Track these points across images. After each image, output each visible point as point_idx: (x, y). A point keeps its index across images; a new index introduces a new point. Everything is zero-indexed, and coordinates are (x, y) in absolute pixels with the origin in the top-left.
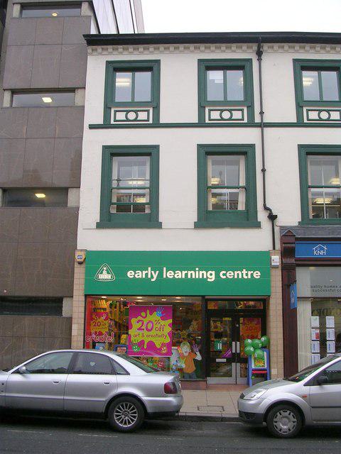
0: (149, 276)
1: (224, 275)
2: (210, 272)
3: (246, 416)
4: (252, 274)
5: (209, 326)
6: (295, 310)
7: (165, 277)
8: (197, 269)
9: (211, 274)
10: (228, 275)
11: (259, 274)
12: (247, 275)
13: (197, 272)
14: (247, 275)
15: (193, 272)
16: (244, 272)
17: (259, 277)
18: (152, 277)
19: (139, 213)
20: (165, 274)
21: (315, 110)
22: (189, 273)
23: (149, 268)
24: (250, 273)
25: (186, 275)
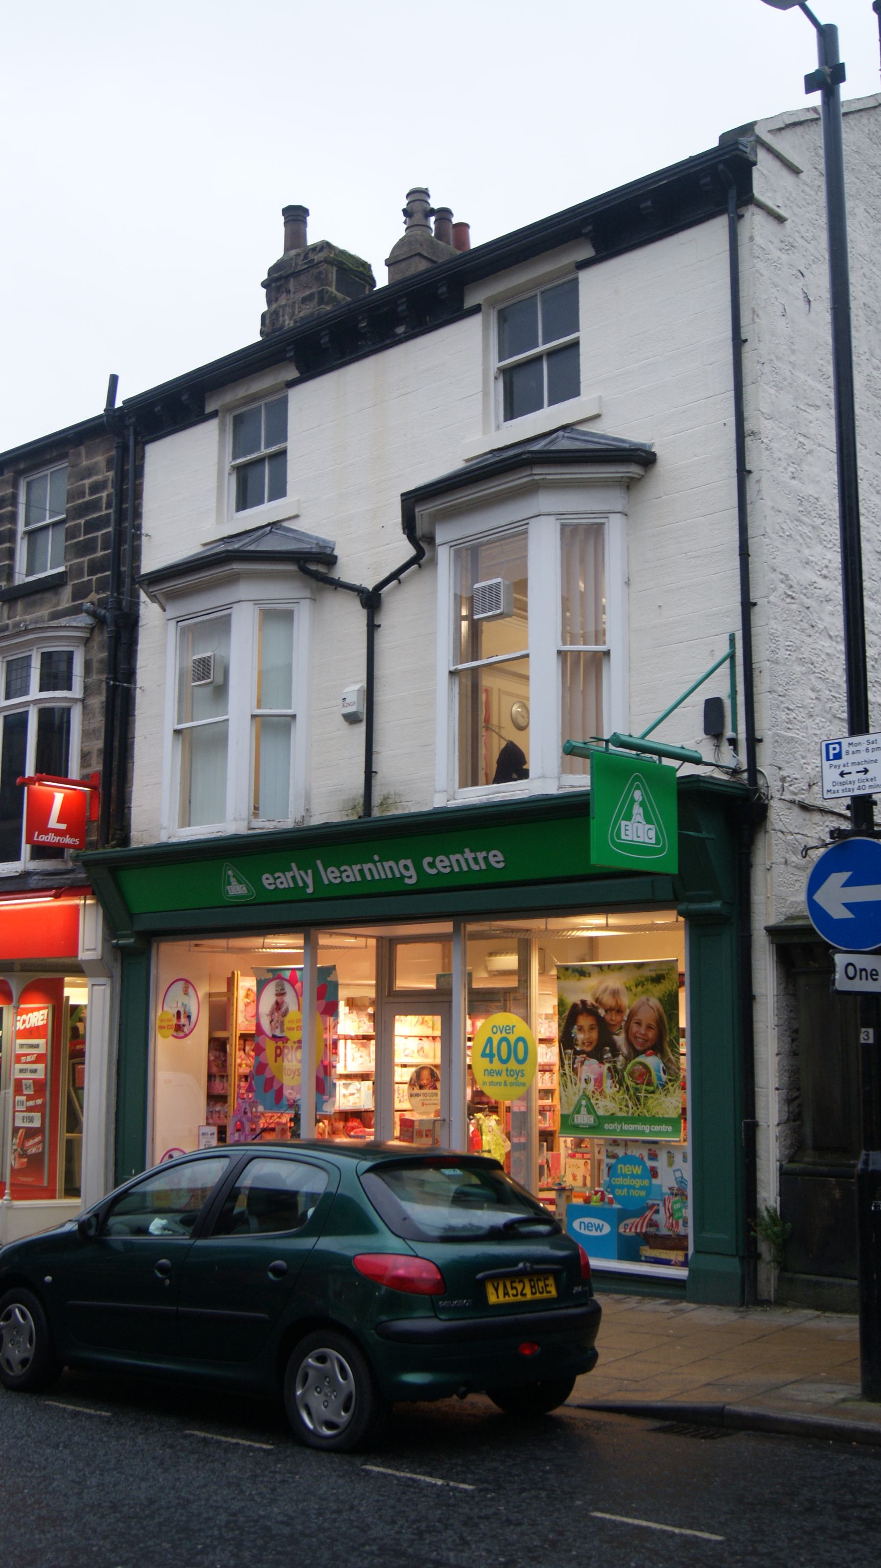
0: (301, 884)
1: (432, 865)
2: (402, 863)
3: (755, 1241)
4: (486, 859)
5: (159, 1211)
6: (202, 417)
7: (326, 882)
8: (376, 858)
9: (406, 867)
10: (439, 865)
11: (500, 857)
12: (475, 860)
13: (379, 864)
14: (475, 860)
15: (371, 865)
16: (468, 854)
17: (502, 865)
18: (306, 885)
19: (770, 1106)
20: (324, 877)
21: (499, 698)
22: (366, 867)
23: (293, 865)
24: (481, 855)
25: (361, 871)
